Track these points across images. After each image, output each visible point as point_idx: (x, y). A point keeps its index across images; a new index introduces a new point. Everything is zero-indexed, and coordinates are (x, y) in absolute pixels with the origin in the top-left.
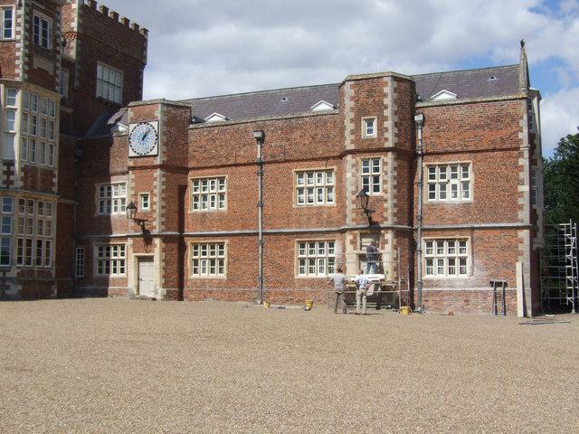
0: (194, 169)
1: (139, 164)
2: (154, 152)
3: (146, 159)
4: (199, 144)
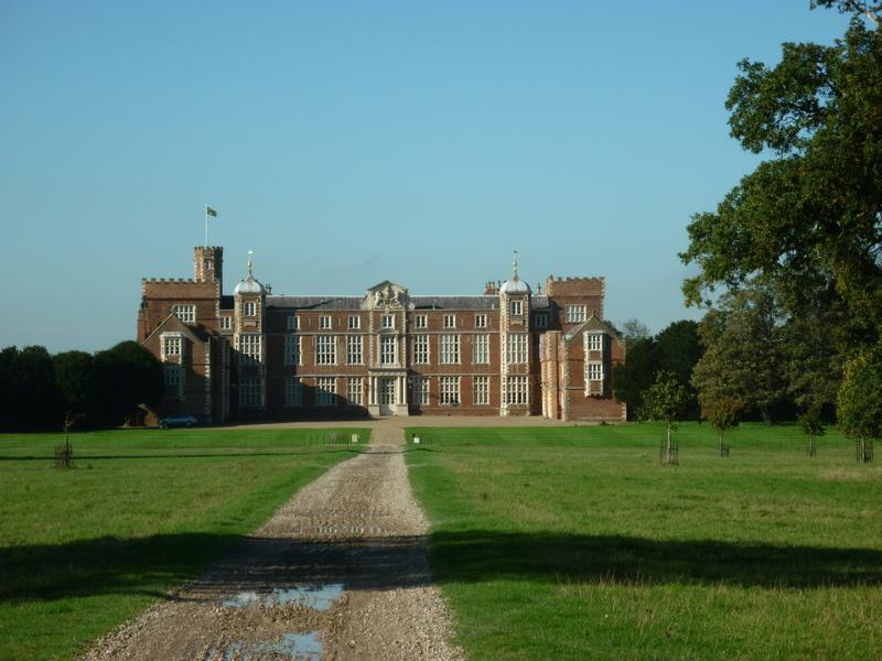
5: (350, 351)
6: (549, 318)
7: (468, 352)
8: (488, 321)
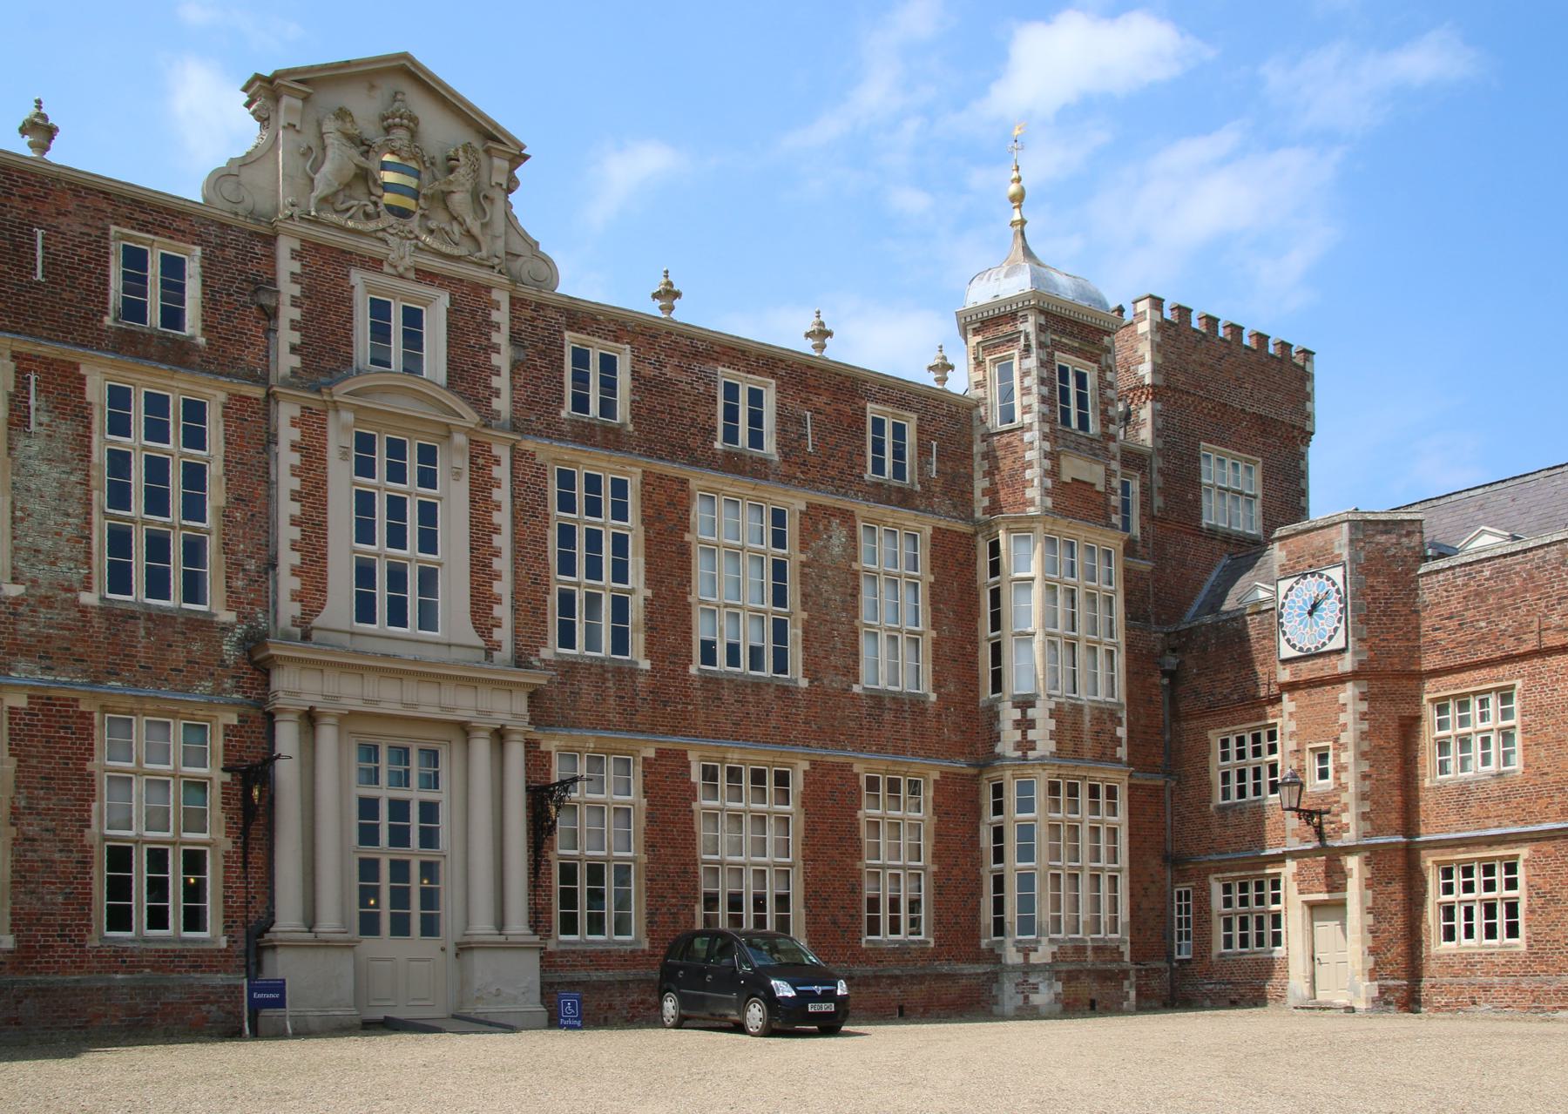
0: (1435, 673)
1: (1304, 676)
2: (1338, 643)
3: (1320, 661)
4: (1444, 611)
5: (120, 497)
6: (1146, 491)
7: (826, 606)
8: (923, 451)
